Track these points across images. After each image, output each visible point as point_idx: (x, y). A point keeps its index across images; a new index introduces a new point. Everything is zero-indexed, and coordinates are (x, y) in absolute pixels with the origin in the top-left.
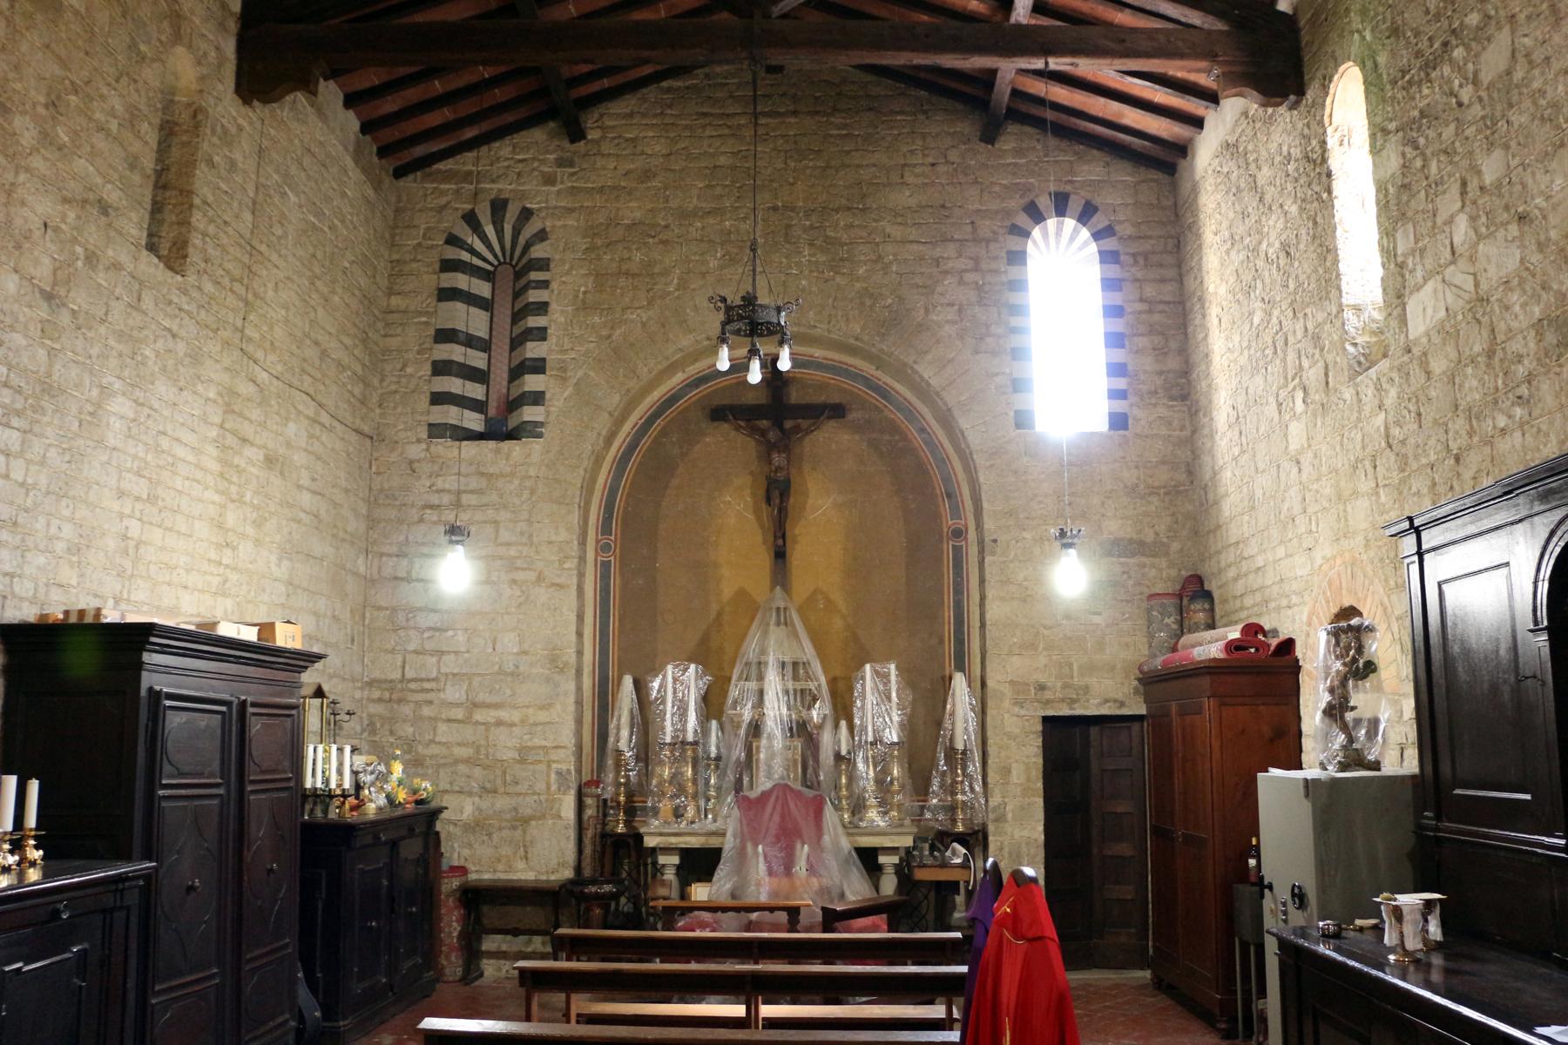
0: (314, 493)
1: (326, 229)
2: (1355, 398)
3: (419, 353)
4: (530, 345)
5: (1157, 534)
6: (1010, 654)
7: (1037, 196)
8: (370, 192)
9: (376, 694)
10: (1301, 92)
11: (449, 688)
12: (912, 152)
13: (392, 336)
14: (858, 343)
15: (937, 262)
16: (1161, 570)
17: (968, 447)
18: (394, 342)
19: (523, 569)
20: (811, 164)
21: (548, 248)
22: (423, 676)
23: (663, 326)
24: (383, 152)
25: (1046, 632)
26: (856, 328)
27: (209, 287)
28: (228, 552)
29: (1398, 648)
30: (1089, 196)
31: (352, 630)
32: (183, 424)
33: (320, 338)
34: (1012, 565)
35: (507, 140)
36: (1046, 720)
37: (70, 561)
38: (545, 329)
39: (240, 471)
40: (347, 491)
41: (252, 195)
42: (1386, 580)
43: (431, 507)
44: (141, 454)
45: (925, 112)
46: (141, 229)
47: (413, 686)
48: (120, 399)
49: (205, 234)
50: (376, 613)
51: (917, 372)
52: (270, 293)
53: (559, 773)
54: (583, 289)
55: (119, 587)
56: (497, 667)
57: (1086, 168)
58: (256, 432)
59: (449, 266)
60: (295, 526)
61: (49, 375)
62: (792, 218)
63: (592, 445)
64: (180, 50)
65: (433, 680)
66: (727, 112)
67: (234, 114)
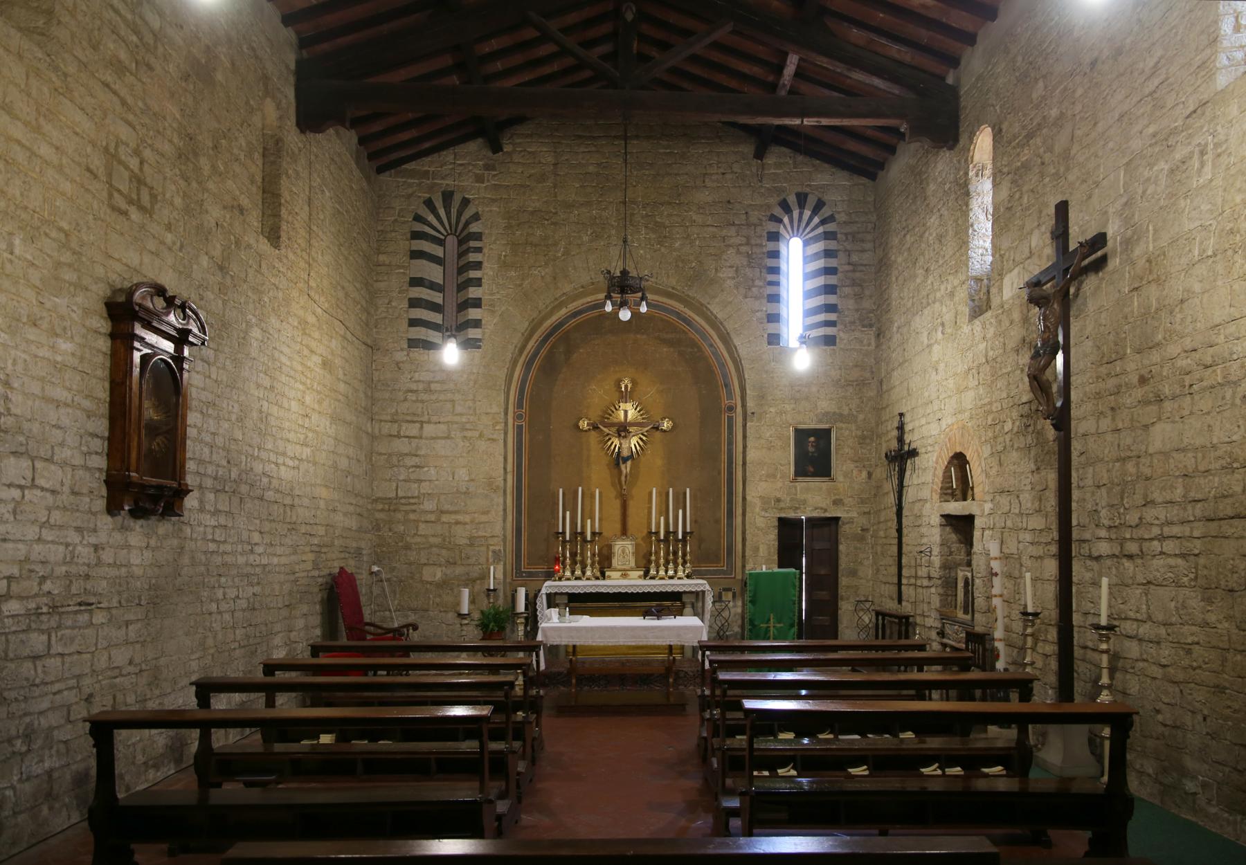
0: (345, 382)
4: (471, 289)
6: (760, 480)
9: (380, 507)
10: (956, 140)
12: (710, 165)
18: (382, 285)
20: (647, 172)
23: (555, 279)
24: (372, 157)
26: (673, 282)
27: (291, 256)
35: (451, 150)
36: (780, 519)
38: (480, 279)
39: (311, 370)
40: (361, 381)
42: (980, 438)
43: (411, 391)
47: (403, 501)
53: (494, 552)
59: (416, 235)
60: (337, 403)
61: (224, 316)
62: (634, 209)
64: (268, 100)
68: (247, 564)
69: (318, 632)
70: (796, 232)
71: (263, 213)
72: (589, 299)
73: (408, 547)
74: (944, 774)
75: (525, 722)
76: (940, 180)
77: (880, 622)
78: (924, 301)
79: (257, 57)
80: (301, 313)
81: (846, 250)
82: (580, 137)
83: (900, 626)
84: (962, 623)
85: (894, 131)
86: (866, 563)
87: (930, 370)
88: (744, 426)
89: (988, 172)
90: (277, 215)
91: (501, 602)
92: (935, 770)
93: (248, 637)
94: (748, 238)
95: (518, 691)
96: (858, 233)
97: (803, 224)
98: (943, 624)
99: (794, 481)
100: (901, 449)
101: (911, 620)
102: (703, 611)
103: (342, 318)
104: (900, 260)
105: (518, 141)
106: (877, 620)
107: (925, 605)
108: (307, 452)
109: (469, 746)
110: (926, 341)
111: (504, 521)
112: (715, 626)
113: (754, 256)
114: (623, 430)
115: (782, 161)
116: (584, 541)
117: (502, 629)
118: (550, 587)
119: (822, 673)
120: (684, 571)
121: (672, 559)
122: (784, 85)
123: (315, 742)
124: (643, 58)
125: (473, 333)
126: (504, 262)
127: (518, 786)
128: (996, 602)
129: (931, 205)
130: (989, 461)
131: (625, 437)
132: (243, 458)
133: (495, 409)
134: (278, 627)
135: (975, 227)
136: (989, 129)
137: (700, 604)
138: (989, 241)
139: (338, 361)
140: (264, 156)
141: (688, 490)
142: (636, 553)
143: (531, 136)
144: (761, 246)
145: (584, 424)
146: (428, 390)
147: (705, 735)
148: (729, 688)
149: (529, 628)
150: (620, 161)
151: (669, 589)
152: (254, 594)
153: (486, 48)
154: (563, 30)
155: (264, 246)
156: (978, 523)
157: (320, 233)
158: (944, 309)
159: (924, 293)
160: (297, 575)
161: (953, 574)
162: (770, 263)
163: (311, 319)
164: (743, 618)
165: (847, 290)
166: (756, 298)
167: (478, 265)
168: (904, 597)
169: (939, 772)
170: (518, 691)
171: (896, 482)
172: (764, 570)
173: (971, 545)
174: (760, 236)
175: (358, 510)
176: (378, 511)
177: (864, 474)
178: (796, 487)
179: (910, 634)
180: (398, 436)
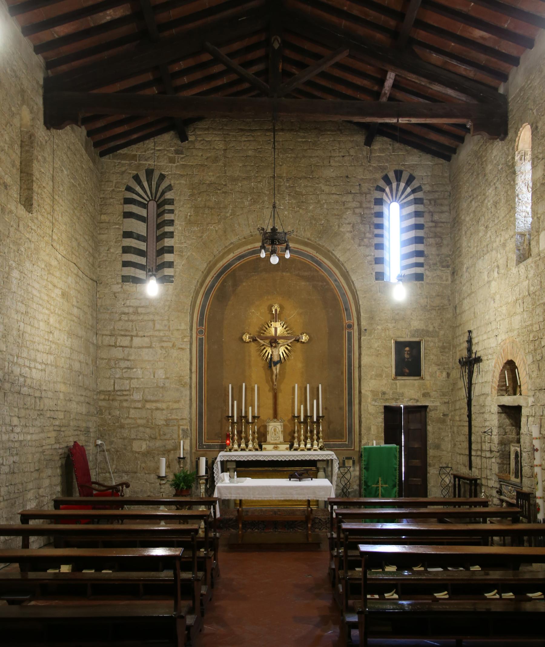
0: (78, 308)
1: (77, 185)
2: (517, 273)
3: (116, 242)
4: (166, 240)
5: (434, 327)
6: (371, 378)
7: (388, 172)
8: (91, 165)
9: (102, 397)
10: (506, 134)
11: (135, 394)
13: (103, 234)
14: (309, 241)
15: (344, 203)
16: (435, 343)
17: (355, 288)
18: (104, 237)
19: (166, 341)
20: (289, 156)
21: (173, 194)
22: (123, 389)
23: (225, 232)
24: (96, 145)
25: (386, 370)
26: (308, 234)
27: (40, 218)
28: (51, 335)
29: (528, 377)
30: (411, 172)
31: (92, 369)
32: (35, 280)
33: (77, 237)
34: (372, 341)
35: (152, 140)
36: (386, 408)
37: (3, 341)
38: (173, 232)
39: (54, 300)
40: (89, 307)
41: (52, 172)
42: (525, 350)
43: (124, 314)
44: (23, 294)
45: (340, 130)
46: (17, 194)
47: (119, 393)
48: (15, 271)
49: (38, 194)
50: (101, 361)
51: (334, 255)
52: (60, 218)
53: (183, 430)
54: (189, 214)
55: (18, 351)
56: (155, 384)
57: (411, 158)
58: (58, 282)
59: (128, 201)
60: (72, 323)
62: (281, 182)
63: (195, 286)
65: (128, 390)
66: (252, 129)
67: (44, 135)
68: (9, 441)
69: (59, 489)
70: (395, 196)
71: (21, 188)
72: (249, 247)
73: (122, 427)
74: (501, 598)
75: (206, 557)
76: (495, 162)
77: (457, 482)
78: (485, 249)
79: (17, 77)
80: (47, 258)
81: (430, 212)
82: (242, 130)
83: (471, 486)
84: (514, 485)
85: (463, 126)
86: (446, 439)
87: (489, 299)
88: (360, 339)
89: (528, 157)
90: (30, 189)
91: (188, 466)
92: (495, 595)
93: (9, 493)
94: (361, 203)
95: (201, 533)
96: (438, 199)
97: (400, 193)
98: (501, 485)
99: (395, 379)
100: (470, 356)
101: (478, 481)
102: (332, 474)
103: (75, 262)
104: (467, 219)
105: (199, 133)
106: (455, 481)
107: (488, 471)
108: (51, 358)
109: (166, 575)
110: (486, 279)
111: (191, 407)
112: (340, 484)
113: (365, 216)
114: (274, 342)
115: (384, 147)
116: (247, 422)
117: (189, 487)
118: (223, 456)
119: (416, 523)
120: (318, 445)
121: (309, 436)
122: (385, 94)
123: (57, 571)
124: (287, 74)
125: (168, 271)
126: (190, 220)
127: (202, 604)
128: (537, 470)
129: (490, 180)
130: (531, 367)
131: (275, 347)
132: (7, 364)
133: (183, 326)
134: (30, 486)
135: (520, 197)
136: (529, 126)
137: (330, 469)
138: (529, 206)
139: (73, 293)
140: (21, 146)
141: (320, 386)
142: (284, 432)
143: (208, 129)
144: (370, 208)
145: (246, 338)
146: (136, 313)
147: (333, 567)
148: (350, 534)
149: (208, 486)
150: (270, 147)
151: (308, 458)
152: (14, 462)
153: (176, 68)
154: (229, 55)
155: (22, 211)
156: (524, 412)
157: (61, 201)
158: (499, 256)
159: (485, 244)
160: (44, 448)
161: (507, 449)
162: (377, 221)
163: (54, 263)
164: (360, 480)
165: (431, 241)
166: (367, 246)
167: (171, 223)
168: (474, 464)
169: (497, 596)
170: (201, 533)
171: (466, 381)
172: (375, 445)
173: (520, 428)
174: (369, 202)
175: (87, 400)
176: (101, 400)
177: (444, 374)
178: (396, 384)
179: (478, 492)
180: (115, 346)
